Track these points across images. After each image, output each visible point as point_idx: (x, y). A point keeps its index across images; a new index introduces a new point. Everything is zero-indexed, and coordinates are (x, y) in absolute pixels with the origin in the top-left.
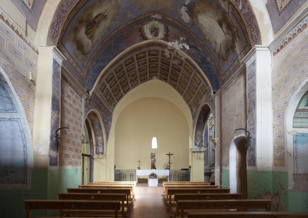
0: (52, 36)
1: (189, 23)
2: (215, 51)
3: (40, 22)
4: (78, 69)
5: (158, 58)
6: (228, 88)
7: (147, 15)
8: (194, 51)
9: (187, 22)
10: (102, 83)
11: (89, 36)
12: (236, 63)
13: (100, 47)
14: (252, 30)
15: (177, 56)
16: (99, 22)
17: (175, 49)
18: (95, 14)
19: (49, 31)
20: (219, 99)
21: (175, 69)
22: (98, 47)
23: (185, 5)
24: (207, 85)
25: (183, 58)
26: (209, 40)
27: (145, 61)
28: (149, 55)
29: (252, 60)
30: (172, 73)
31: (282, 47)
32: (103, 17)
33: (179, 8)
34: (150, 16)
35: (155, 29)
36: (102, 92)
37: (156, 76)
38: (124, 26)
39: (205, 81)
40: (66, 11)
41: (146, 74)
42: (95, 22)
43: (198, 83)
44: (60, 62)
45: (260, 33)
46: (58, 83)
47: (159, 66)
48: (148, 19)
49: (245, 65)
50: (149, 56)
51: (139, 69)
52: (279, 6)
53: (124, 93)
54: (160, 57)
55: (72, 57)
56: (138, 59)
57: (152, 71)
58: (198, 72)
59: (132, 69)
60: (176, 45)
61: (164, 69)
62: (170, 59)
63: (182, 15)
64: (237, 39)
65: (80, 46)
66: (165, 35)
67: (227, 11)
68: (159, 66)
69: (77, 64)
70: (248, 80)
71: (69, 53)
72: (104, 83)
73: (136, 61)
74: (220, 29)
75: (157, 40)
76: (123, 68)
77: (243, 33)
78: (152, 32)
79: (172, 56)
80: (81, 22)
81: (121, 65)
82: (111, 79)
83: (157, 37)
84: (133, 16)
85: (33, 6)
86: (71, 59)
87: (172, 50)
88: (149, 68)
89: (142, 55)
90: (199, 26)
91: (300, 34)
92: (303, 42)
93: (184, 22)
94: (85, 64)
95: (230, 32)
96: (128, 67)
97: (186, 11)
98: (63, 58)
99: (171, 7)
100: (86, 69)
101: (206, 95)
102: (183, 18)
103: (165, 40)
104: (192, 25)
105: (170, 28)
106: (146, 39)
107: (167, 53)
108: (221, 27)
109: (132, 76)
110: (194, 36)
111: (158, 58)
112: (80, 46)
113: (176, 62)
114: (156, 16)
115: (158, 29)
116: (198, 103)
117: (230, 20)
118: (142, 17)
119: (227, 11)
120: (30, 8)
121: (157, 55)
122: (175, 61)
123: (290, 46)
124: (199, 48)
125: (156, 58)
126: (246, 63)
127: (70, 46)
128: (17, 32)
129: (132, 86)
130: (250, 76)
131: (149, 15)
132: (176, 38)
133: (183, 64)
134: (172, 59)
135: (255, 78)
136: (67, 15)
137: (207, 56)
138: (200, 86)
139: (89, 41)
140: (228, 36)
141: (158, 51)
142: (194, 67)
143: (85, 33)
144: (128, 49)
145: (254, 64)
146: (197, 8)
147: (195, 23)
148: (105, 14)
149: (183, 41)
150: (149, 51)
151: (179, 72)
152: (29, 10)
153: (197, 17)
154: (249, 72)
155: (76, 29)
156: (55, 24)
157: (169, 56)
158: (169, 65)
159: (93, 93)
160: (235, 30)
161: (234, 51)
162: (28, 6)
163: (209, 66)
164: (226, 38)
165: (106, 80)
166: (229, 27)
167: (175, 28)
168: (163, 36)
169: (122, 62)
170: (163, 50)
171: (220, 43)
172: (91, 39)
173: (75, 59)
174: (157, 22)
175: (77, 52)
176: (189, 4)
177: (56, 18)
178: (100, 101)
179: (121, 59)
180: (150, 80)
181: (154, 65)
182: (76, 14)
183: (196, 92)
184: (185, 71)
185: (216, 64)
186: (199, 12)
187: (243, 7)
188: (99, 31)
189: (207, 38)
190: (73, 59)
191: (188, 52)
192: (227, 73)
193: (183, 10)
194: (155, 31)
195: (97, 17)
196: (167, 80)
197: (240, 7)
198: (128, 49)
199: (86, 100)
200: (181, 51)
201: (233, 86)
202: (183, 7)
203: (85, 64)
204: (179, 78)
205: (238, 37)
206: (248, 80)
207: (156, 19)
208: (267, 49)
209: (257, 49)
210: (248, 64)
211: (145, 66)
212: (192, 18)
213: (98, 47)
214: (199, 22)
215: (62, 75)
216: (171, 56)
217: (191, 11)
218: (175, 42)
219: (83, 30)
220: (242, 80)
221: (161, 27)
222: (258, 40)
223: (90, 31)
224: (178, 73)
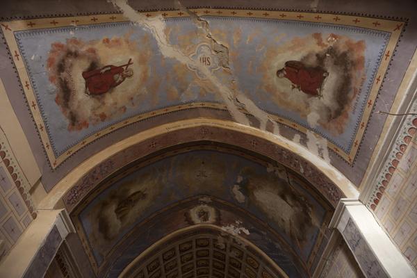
0: (66, 201)
2: (284, 231)
3: (59, 184)
4: (92, 258)
5: (208, 269)
11: (120, 216)
12: (319, 240)
13: (132, 232)
14: (326, 189)
15: (235, 244)
16: (136, 201)
17: (231, 234)
18: (133, 191)
19: (66, 194)
21: (234, 265)
22: (129, 232)
23: (237, 184)
25: (243, 247)
27: (190, 256)
28: (197, 246)
29: (344, 219)
30: (229, 272)
31: (379, 195)
34: (198, 199)
35: (204, 213)
40: (97, 179)
42: (131, 200)
44: (64, 233)
45: (338, 188)
46: (46, 265)
47: (211, 271)
48: (197, 203)
49: (337, 231)
50: (196, 247)
51: (182, 268)
52: (347, 160)
54: (211, 249)
55: (88, 240)
56: (181, 251)
57: (201, 271)
58: (268, 264)
59: (171, 268)
60: (232, 230)
61: (217, 268)
62: (225, 250)
64: (310, 209)
65: (104, 226)
66: (216, 219)
67: (287, 181)
68: (211, 271)
69: (92, 251)
70: (354, 249)
71: (85, 233)
73: (178, 255)
74: (285, 202)
75: (206, 225)
76: (159, 264)
77: (318, 200)
78: (200, 216)
79: (228, 246)
80: (113, 197)
81: (158, 259)
83: (207, 222)
85: (58, 167)
86: (86, 242)
87: (227, 236)
88: (198, 266)
89: (187, 246)
91: (395, 172)
92: (407, 179)
93: (238, 203)
94: (105, 254)
95: (297, 202)
96: (166, 263)
97: (239, 190)
98: (70, 227)
100: (105, 262)
102: (237, 198)
103: (217, 225)
105: (222, 211)
106: (193, 223)
107: (221, 242)
108: (286, 200)
112: (104, 226)
113: (233, 254)
114: (205, 199)
117: (293, 190)
118: (189, 200)
119: (287, 181)
120: (54, 168)
121: (207, 246)
122: (232, 252)
123: (390, 189)
124: (263, 232)
125: (206, 260)
126: (338, 228)
127: (90, 224)
128: (18, 184)
130: (355, 243)
131: (197, 197)
132: (230, 222)
133: (245, 256)
134: (228, 250)
135: (365, 242)
136: (97, 183)
137: (276, 242)
140: (296, 209)
142: (261, 257)
143: (116, 211)
144: (169, 236)
145: (351, 223)
146: (251, 184)
149: (240, 225)
152: (52, 169)
153: (253, 195)
154: (349, 238)
155: (105, 205)
156: (78, 189)
157: (223, 247)
158: (225, 260)
160: (303, 199)
161: (311, 225)
162: (52, 165)
163: (280, 254)
164: (295, 211)
166: (295, 197)
167: (228, 209)
168: (214, 221)
169: (159, 254)
171: (288, 219)
172: (121, 221)
173: (91, 244)
174: (206, 206)
176: (241, 182)
177: (82, 182)
179: (157, 249)
181: (204, 262)
182: (109, 187)
184: (248, 266)
185: (291, 249)
187: (306, 169)
188: (133, 213)
189: (271, 217)
190: (89, 243)
191: (248, 238)
192: (312, 259)
193: (236, 189)
194: (204, 215)
195: (134, 194)
197: (302, 171)
198: (169, 236)
200: (240, 237)
201: (330, 272)
203: (105, 254)
205: (311, 206)
206: (354, 249)
207: (204, 203)
208: (358, 202)
209: (345, 203)
210: (341, 227)
211: (191, 263)
213: (129, 232)
215: (57, 256)
216: (226, 246)
217: (245, 189)
218: (229, 226)
219: (114, 207)
220: (341, 256)
221: (212, 212)
222: (339, 194)
223: (123, 209)
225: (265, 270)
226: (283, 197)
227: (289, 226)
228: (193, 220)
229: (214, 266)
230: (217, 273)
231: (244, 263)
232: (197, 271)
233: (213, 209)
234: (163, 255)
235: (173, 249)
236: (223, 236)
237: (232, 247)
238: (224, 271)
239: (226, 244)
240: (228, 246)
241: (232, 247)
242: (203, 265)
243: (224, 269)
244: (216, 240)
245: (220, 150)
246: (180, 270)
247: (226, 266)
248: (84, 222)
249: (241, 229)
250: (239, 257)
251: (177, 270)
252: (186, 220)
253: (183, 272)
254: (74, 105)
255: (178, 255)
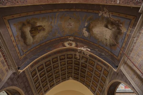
1: (88, 36)
6: (132, 49)
7: (66, 37)
8: (93, 51)
9: (87, 36)
10: (33, 69)
11: (32, 35)
16: (40, 30)
18: (38, 24)
20: (125, 66)
23: (85, 27)
24: (108, 67)
25: (88, 56)
26: (101, 41)
32: (42, 29)
33: (82, 30)
35: (70, 44)
36: (33, 77)
37: (71, 77)
38: (54, 40)
39: (105, 65)
41: (65, 74)
42: (37, 29)
43: (100, 70)
47: (73, 71)
52: (117, 59)
53: (51, 87)
54: (73, 60)
58: (99, 61)
62: (79, 59)
63: (84, 33)
64: (121, 25)
67: (109, 17)
68: (73, 71)
69: (17, 45)
72: (35, 70)
73: (59, 61)
79: (81, 57)
80: (28, 23)
82: (43, 75)
84: (59, 36)
87: (81, 52)
88: (68, 69)
89: (63, 57)
90: (94, 35)
94: (25, 51)
97: (86, 30)
99: (78, 30)
100: (24, 55)
101: (108, 77)
102: (85, 35)
104: (90, 37)
106: (65, 46)
109: (56, 73)
110: (92, 42)
111: (72, 60)
115: (72, 44)
116: (103, 89)
117: (112, 20)
118: (64, 38)
120: (3, 17)
129: (56, 83)
138: (102, 72)
139: (31, 38)
140: (113, 29)
141: (72, 54)
142: (96, 58)
144: (55, 50)
146: (92, 25)
147: (91, 35)
148: (44, 28)
150: (67, 55)
151: (86, 67)
153: (92, 30)
158: (79, 65)
159: (24, 72)
162: (4, 17)
165: (38, 68)
166: (112, 24)
167: (81, 40)
170: (75, 54)
175: (20, 38)
178: (28, 83)
180: (68, 79)
183: (100, 79)
185: (110, 53)
186: (93, 27)
188: (40, 35)
191: (90, 51)
195: (39, 26)
196: (78, 79)
199: (14, 73)
200: (86, 51)
202: (84, 28)
203: (25, 51)
204: (86, 73)
207: (71, 40)
212: (90, 32)
214: (94, 33)
217: (89, 29)
223: (33, 32)
224: (85, 69)
225: (98, 64)
226: (106, 26)
227: (109, 41)
228: (66, 45)
229: (74, 69)
230: (76, 72)
231: (88, 64)
232: (67, 71)
233: (74, 43)
234: (53, 59)
235: (57, 58)
236: (79, 52)
237: (83, 57)
238: (79, 71)
239: (80, 56)
240: (81, 57)
241: (83, 57)
242: (70, 68)
243: (79, 70)
244: (75, 55)
245: (78, 11)
246: (60, 69)
247: (80, 68)
248: (11, 25)
249: (87, 49)
250: (86, 62)
251: (59, 74)
252: (63, 45)
253: (61, 71)
254: (28, 41)
255: (59, 61)
